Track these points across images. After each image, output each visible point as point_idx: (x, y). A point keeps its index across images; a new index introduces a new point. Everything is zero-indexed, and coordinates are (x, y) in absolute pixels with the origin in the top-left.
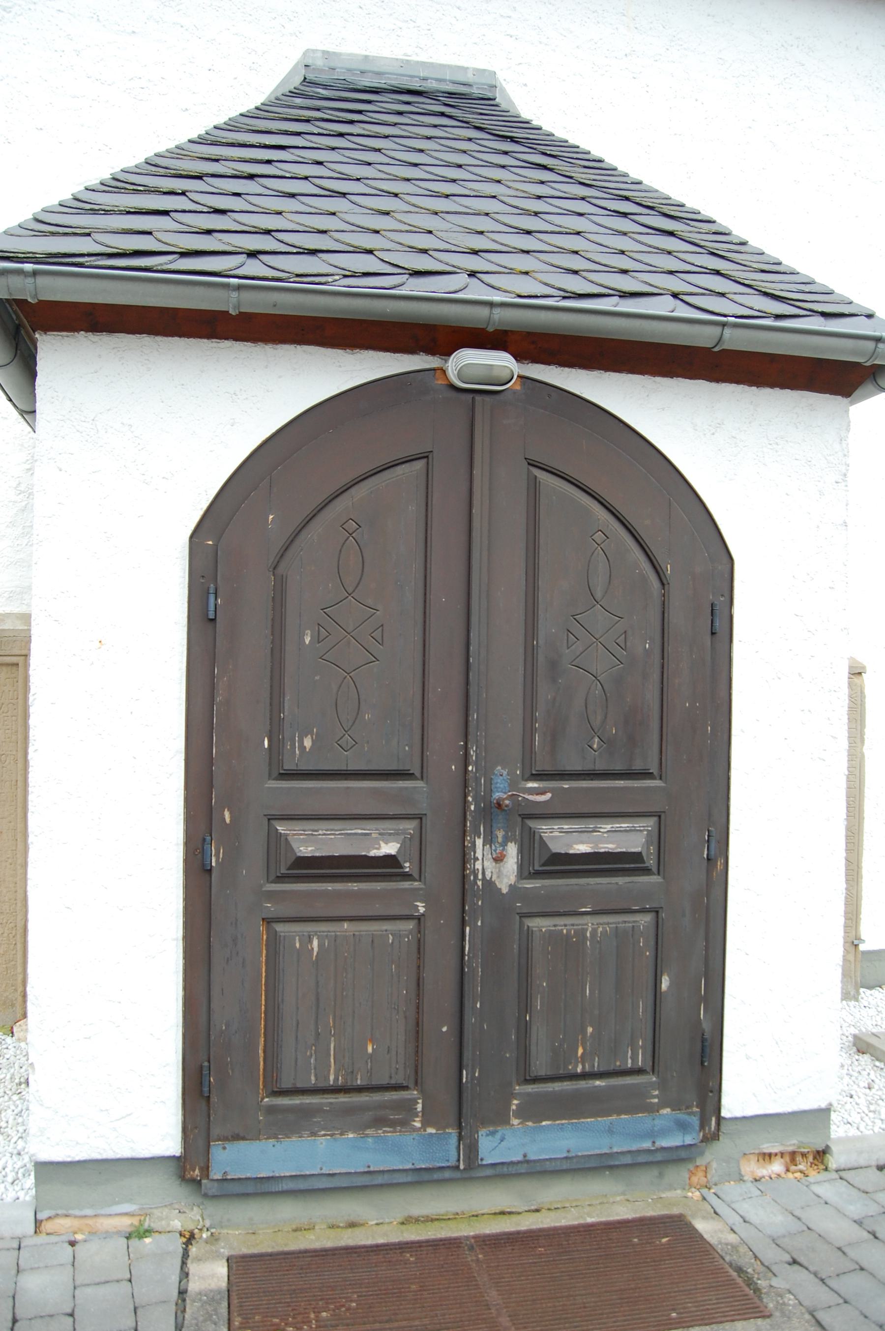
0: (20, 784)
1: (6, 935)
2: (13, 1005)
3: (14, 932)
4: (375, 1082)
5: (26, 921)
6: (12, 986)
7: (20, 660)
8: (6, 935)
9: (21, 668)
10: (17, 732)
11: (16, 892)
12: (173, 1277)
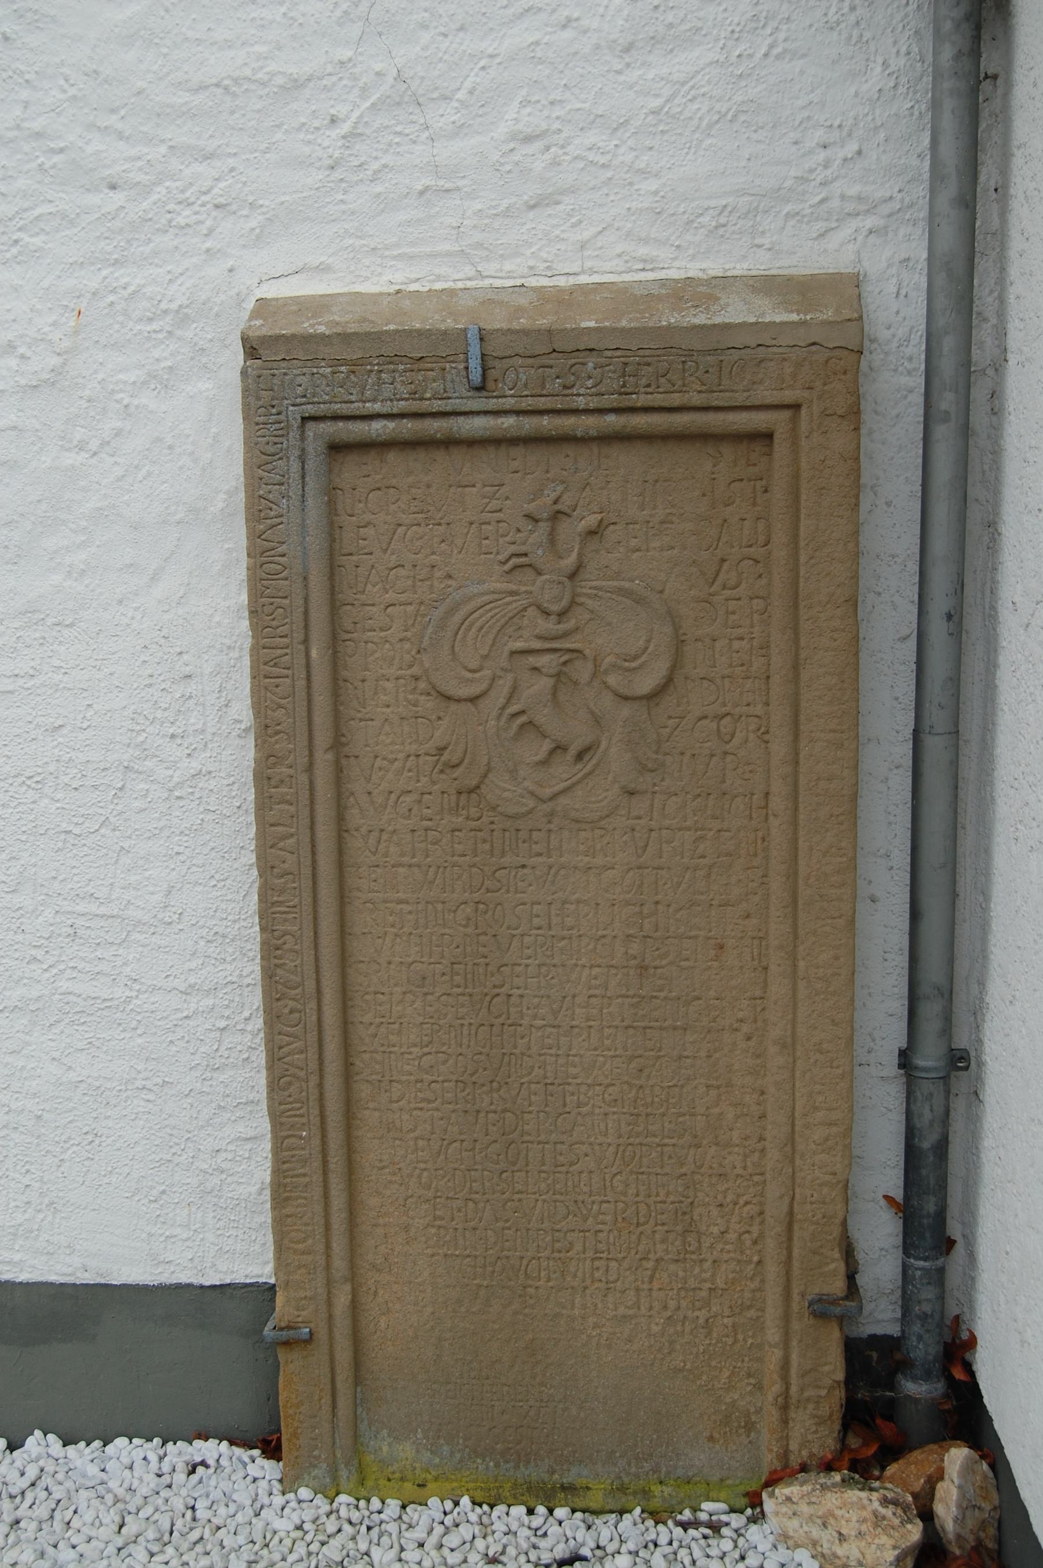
0: (777, 803)
1: (732, 1236)
2: (749, 1427)
3: (755, 1230)
4: (909, 762)
5: (940, 1069)
6: (749, 1375)
7: (777, 421)
8: (732, 1236)
9: (781, 448)
10: (766, 646)
11: (763, 1116)
12: (253, 1470)
